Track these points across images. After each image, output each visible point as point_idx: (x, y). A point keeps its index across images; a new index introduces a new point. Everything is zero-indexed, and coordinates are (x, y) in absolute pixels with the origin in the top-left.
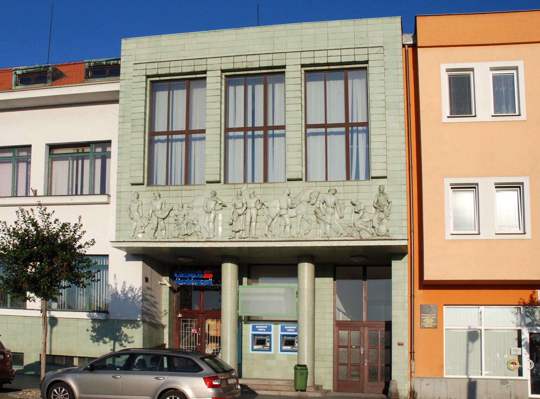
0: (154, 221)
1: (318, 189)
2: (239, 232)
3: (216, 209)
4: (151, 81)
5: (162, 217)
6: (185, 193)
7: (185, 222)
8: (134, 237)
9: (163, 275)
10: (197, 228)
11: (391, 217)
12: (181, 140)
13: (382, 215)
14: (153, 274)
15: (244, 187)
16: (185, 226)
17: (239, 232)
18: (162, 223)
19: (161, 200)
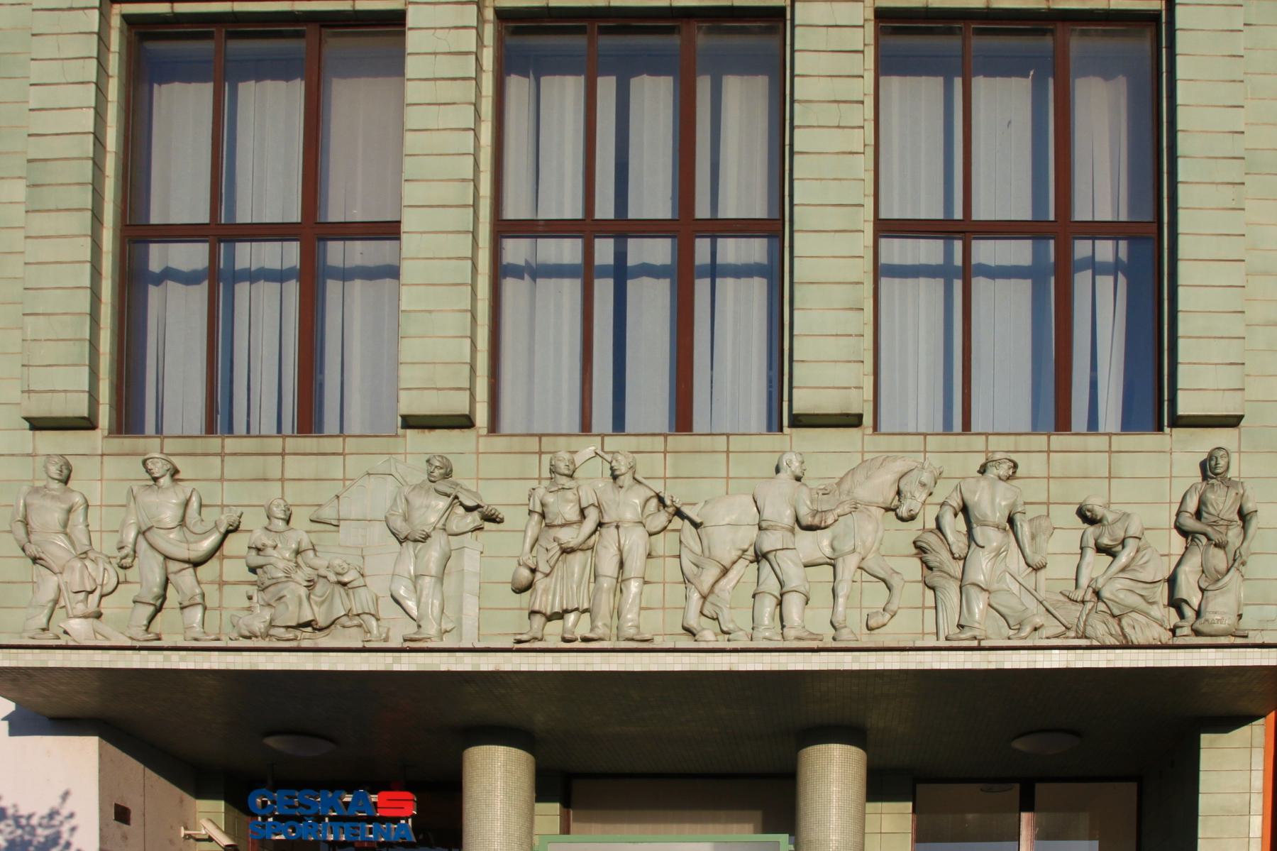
0: (150, 571)
1: (934, 460)
2: (560, 615)
3: (454, 526)
4: (128, 19)
5: (184, 554)
6: (294, 466)
7: (301, 576)
8: (49, 634)
9: (201, 792)
10: (361, 600)
11: (1255, 566)
12: (279, 276)
13: (1219, 559)
14: (149, 789)
15: (588, 447)
16: (303, 592)
17: (560, 615)
18: (186, 579)
19: (183, 490)
